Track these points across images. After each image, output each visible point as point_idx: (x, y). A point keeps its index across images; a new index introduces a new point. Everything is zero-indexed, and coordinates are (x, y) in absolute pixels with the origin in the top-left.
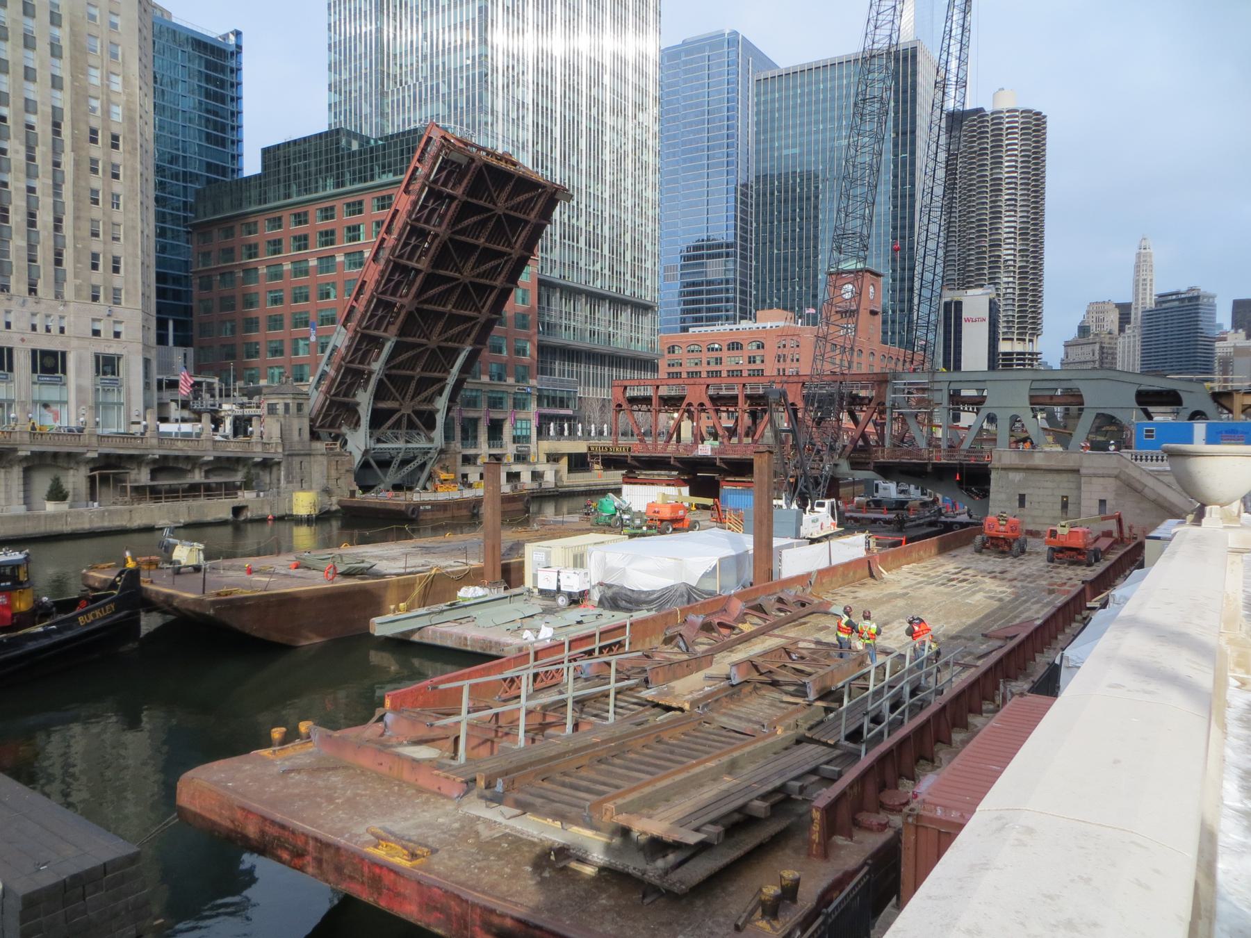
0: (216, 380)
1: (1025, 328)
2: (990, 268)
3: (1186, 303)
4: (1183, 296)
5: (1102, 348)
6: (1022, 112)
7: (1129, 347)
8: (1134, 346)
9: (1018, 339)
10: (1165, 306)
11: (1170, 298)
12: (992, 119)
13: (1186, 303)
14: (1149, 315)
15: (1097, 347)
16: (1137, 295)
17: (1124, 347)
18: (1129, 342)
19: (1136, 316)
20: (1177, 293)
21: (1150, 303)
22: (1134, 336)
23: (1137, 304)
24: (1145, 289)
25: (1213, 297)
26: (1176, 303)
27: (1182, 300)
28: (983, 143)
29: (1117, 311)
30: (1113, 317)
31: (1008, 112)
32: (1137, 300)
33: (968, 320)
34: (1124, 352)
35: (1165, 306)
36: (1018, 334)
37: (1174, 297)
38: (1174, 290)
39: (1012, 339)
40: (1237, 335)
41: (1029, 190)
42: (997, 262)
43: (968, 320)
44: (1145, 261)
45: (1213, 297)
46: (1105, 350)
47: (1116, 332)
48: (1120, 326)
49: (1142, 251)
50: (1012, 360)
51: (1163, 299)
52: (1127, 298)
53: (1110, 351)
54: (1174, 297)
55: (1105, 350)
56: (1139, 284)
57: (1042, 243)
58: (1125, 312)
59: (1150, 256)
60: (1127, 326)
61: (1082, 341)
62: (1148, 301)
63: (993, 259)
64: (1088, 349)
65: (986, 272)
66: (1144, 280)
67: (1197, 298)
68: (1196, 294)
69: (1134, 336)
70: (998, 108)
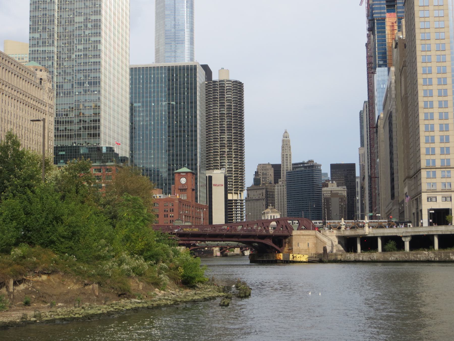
0: (410, 224)
1: (238, 187)
2: (220, 157)
3: (308, 169)
4: (306, 165)
5: (267, 192)
6: (233, 82)
7: (281, 191)
8: (283, 194)
9: (235, 193)
10: (297, 169)
11: (300, 166)
12: (220, 84)
13: (308, 169)
14: (289, 174)
15: (264, 191)
16: (283, 160)
17: (278, 192)
18: (281, 189)
19: (284, 174)
20: (303, 163)
21: (290, 168)
22: (283, 186)
23: (283, 165)
24: (287, 160)
25: (320, 166)
26: (303, 168)
27: (305, 167)
28: (215, 95)
29: (273, 169)
30: (271, 172)
31: (227, 81)
32: (283, 163)
33: (215, 185)
34: (278, 194)
35: (297, 169)
36: (234, 190)
37: (302, 165)
38: (301, 161)
39: (232, 193)
40: (333, 184)
41: (237, 119)
42: (223, 154)
43: (215, 185)
44: (287, 144)
45: (320, 166)
46: (268, 193)
47: (273, 182)
48: (275, 180)
49: (285, 139)
50: (232, 203)
51: (296, 166)
52: (278, 161)
53: (271, 193)
54: (302, 165)
55: (268, 193)
56: (286, 155)
57: (184, 66)
58: (277, 168)
59: (289, 142)
60: (279, 180)
61: (256, 187)
62: (289, 166)
63: (222, 153)
64: (260, 192)
65: (218, 159)
66: (287, 155)
67: (312, 166)
68: (312, 164)
69: (283, 186)
70: (222, 79)
